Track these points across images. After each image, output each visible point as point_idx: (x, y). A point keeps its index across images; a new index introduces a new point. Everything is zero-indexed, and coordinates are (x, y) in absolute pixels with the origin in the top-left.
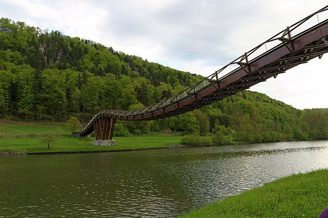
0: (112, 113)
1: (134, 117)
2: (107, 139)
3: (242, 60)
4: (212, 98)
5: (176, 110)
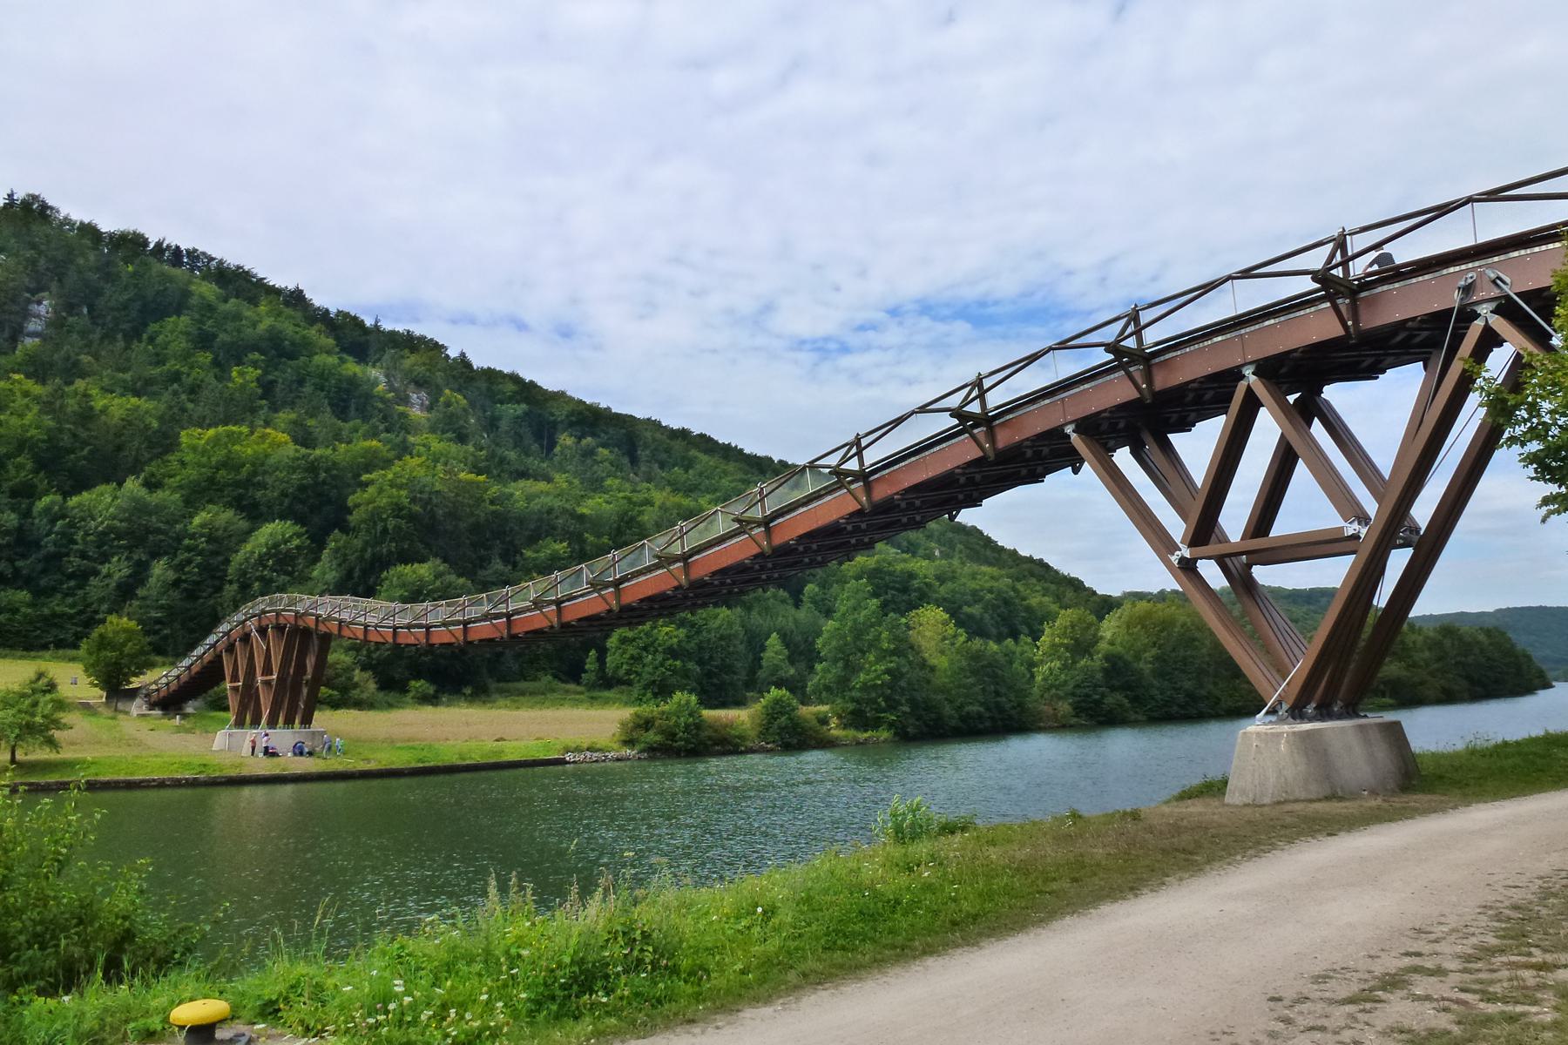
0: (345, 616)
1: (428, 632)
2: (289, 722)
3: (845, 459)
4: (746, 577)
5: (610, 611)
